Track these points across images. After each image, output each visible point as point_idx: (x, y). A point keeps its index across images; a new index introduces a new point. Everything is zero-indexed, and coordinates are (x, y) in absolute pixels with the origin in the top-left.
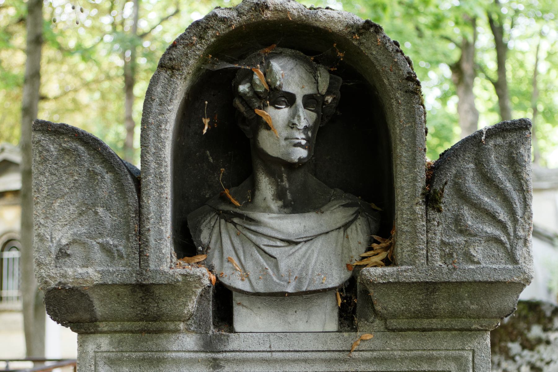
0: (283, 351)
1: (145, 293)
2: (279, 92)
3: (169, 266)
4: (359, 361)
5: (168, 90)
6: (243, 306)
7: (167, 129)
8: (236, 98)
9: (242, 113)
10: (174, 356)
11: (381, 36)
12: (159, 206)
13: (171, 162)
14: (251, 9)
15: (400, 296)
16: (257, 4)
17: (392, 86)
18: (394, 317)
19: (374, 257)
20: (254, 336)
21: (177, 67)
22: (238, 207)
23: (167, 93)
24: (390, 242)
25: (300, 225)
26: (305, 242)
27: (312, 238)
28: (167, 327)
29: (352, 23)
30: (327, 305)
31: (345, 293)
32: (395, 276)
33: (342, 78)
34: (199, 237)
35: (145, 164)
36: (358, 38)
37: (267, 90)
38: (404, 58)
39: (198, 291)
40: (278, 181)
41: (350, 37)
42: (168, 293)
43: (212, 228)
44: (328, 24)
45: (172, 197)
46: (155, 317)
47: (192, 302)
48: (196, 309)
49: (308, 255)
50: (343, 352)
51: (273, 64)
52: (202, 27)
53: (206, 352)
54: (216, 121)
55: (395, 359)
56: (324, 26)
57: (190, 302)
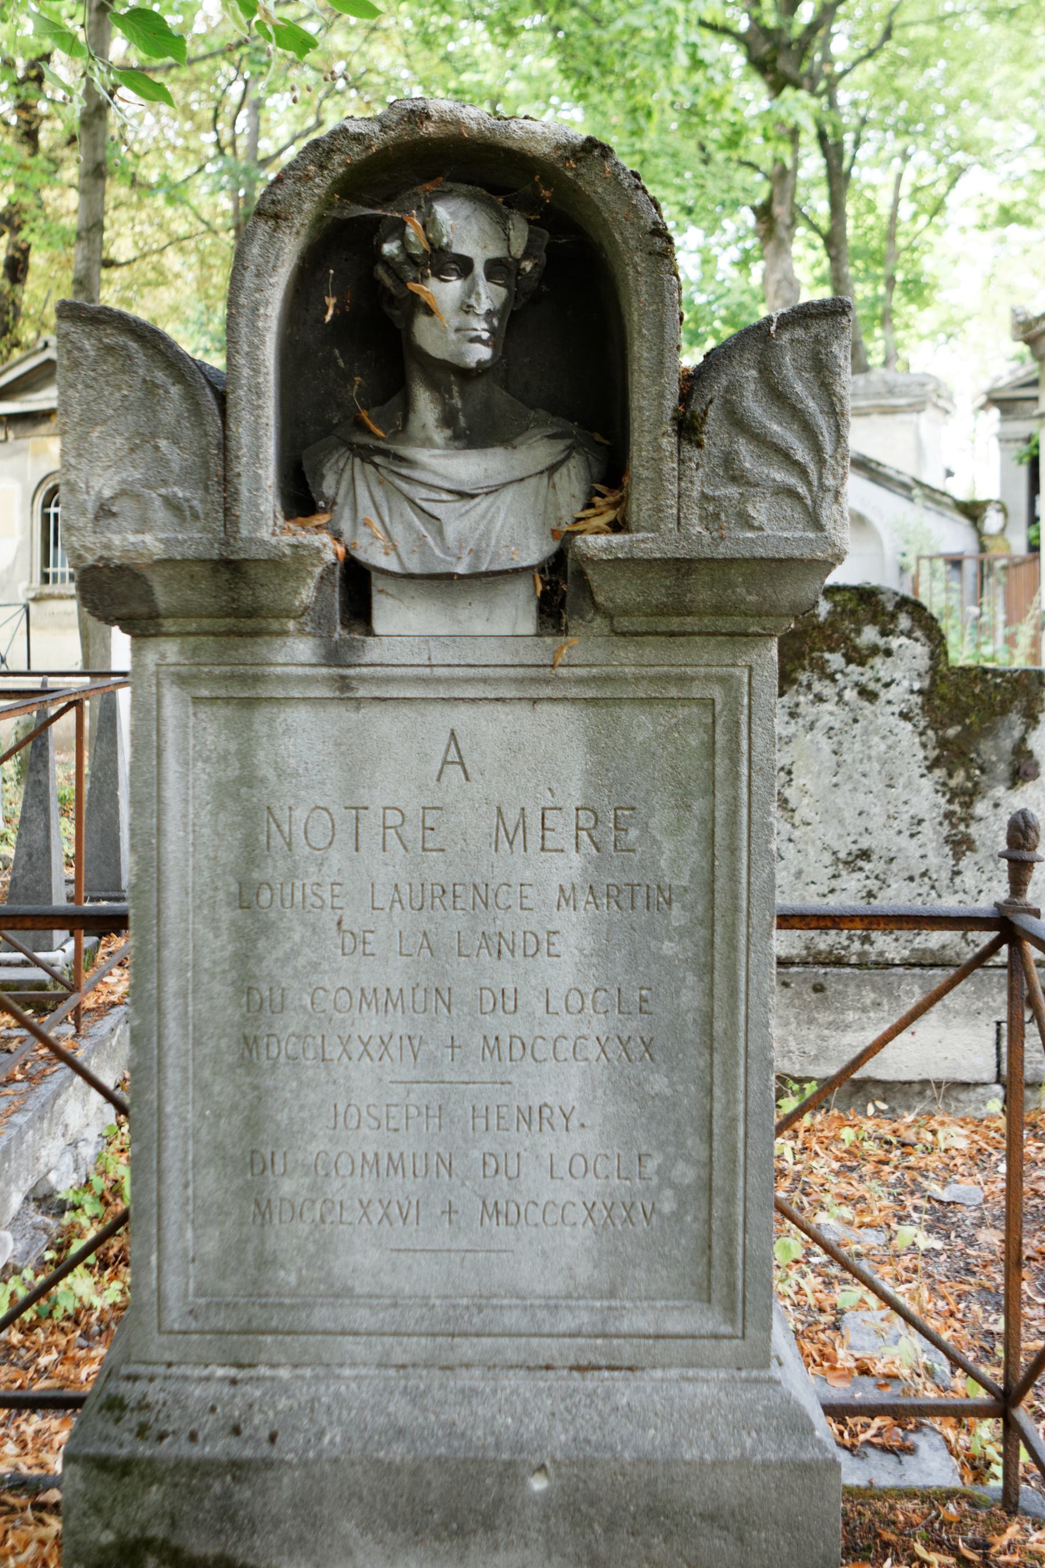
0: (449, 666)
6: (387, 594)
9: (389, 290)
16: (412, 111)
18: (625, 612)
22: (383, 439)
26: (487, 494)
34: (320, 485)
53: (330, 666)
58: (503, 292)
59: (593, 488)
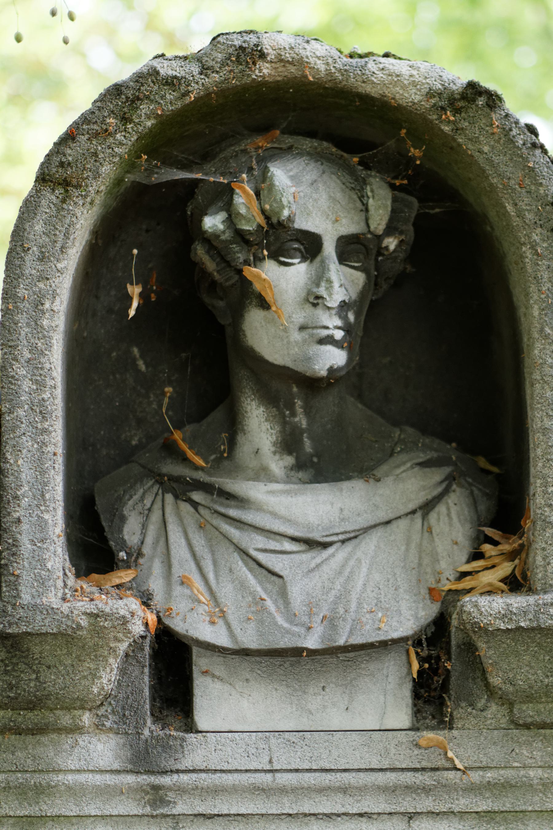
0: (297, 771)
1: (10, 652)
2: (288, 231)
3: (60, 595)
4: (456, 790)
5: (57, 229)
6: (213, 676)
7: (55, 309)
8: (197, 243)
9: (210, 275)
10: (71, 781)
11: (501, 115)
12: (40, 472)
13: (62, 377)
14: (229, 59)
15: (542, 656)
16: (241, 47)
17: (523, 218)
18: (529, 698)
19: (485, 572)
20: (238, 738)
21: (74, 182)
22: (202, 469)
23: (55, 235)
24: (521, 542)
25: (332, 507)
26: (343, 542)
27: (357, 533)
28: (56, 721)
29: (440, 87)
30: (390, 673)
31: (425, 648)
32: (531, 616)
33: (417, 198)
34: (120, 530)
35: (10, 382)
36: (452, 118)
37: (263, 228)
38: (548, 160)
39: (121, 648)
40: (284, 413)
41: (435, 117)
42: (59, 652)
43: (146, 512)
44: (389, 90)
45: (64, 450)
46: (31, 702)
47: (108, 670)
48: (116, 683)
49: (348, 570)
50: (423, 773)
51: (275, 172)
52: (127, 98)
53: (138, 773)
54: (155, 288)
55: (531, 786)
56: (381, 92)
57: (103, 670)
58: (360, 278)
59: (480, 532)
